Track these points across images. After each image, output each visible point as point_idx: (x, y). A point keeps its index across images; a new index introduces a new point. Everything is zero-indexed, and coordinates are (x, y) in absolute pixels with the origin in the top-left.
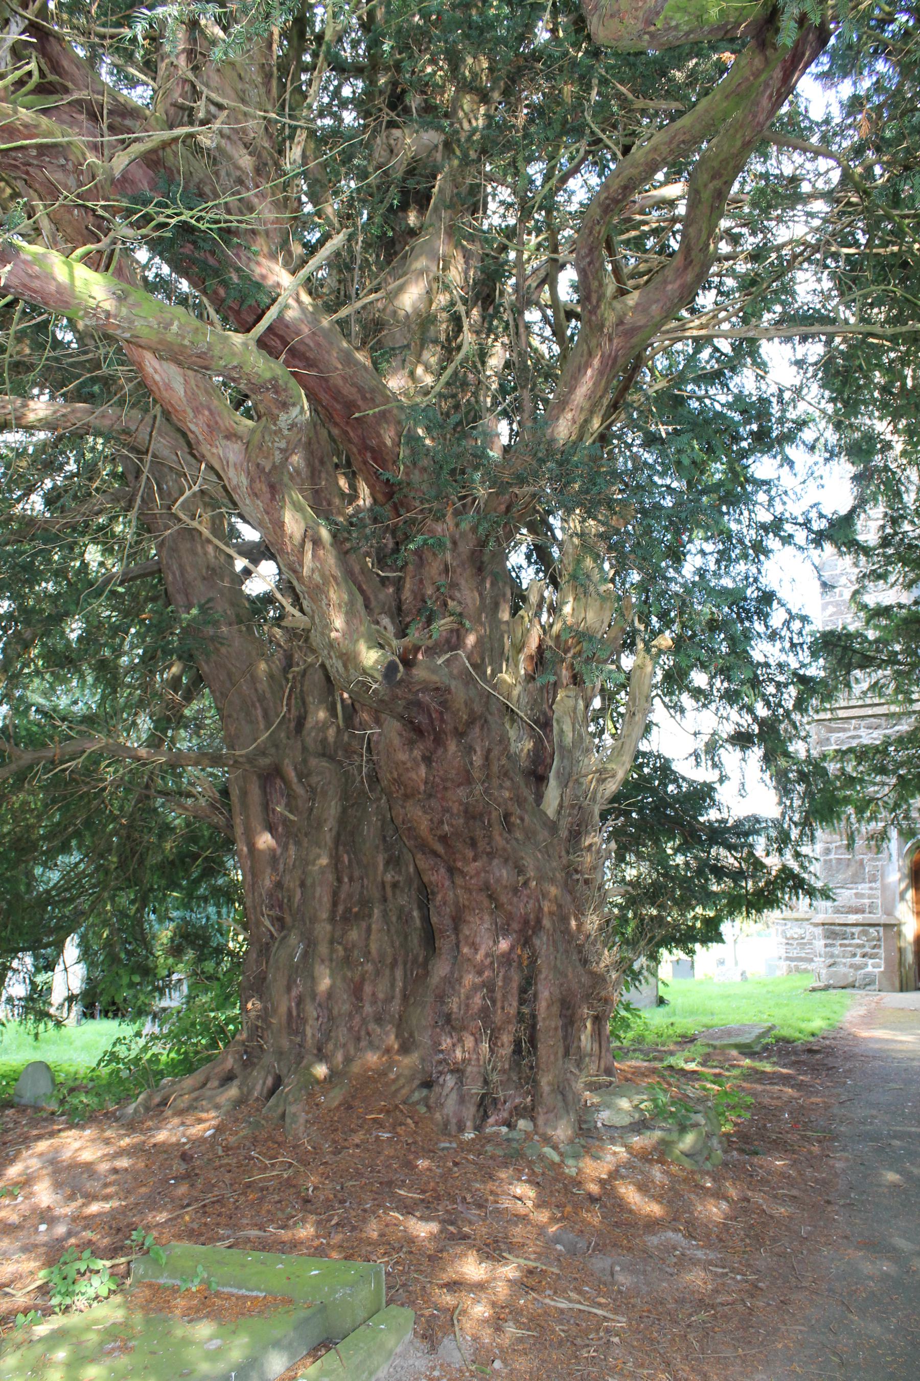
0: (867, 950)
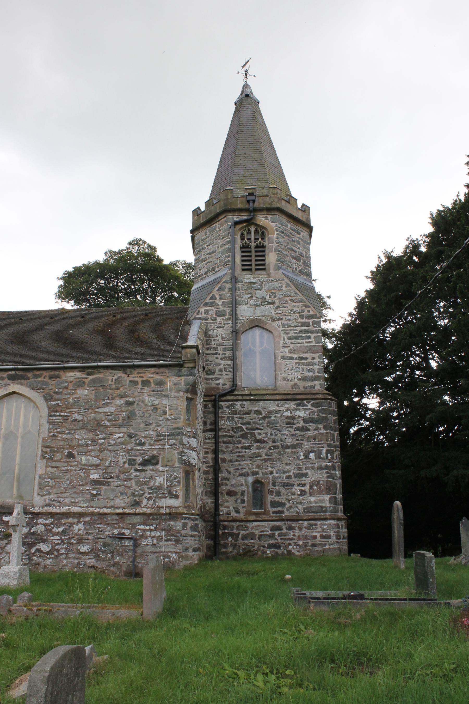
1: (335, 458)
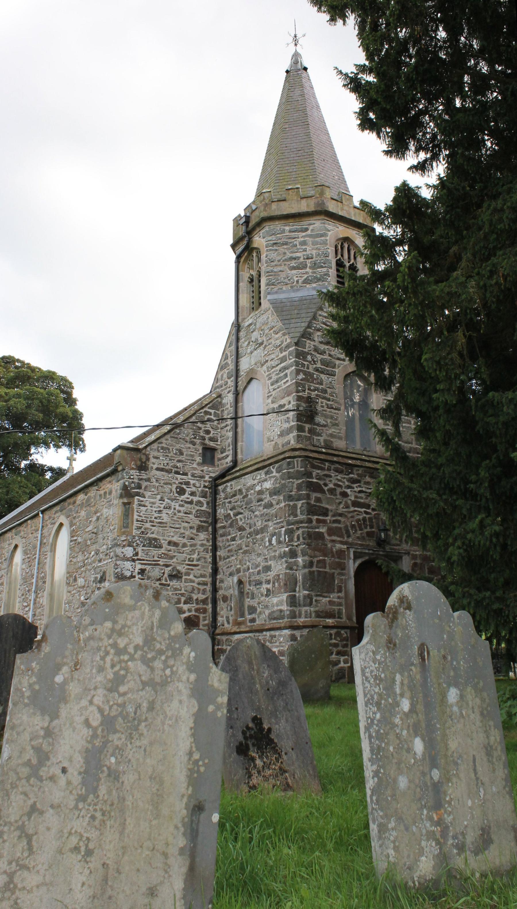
0: (340, 648)
1: (296, 540)
